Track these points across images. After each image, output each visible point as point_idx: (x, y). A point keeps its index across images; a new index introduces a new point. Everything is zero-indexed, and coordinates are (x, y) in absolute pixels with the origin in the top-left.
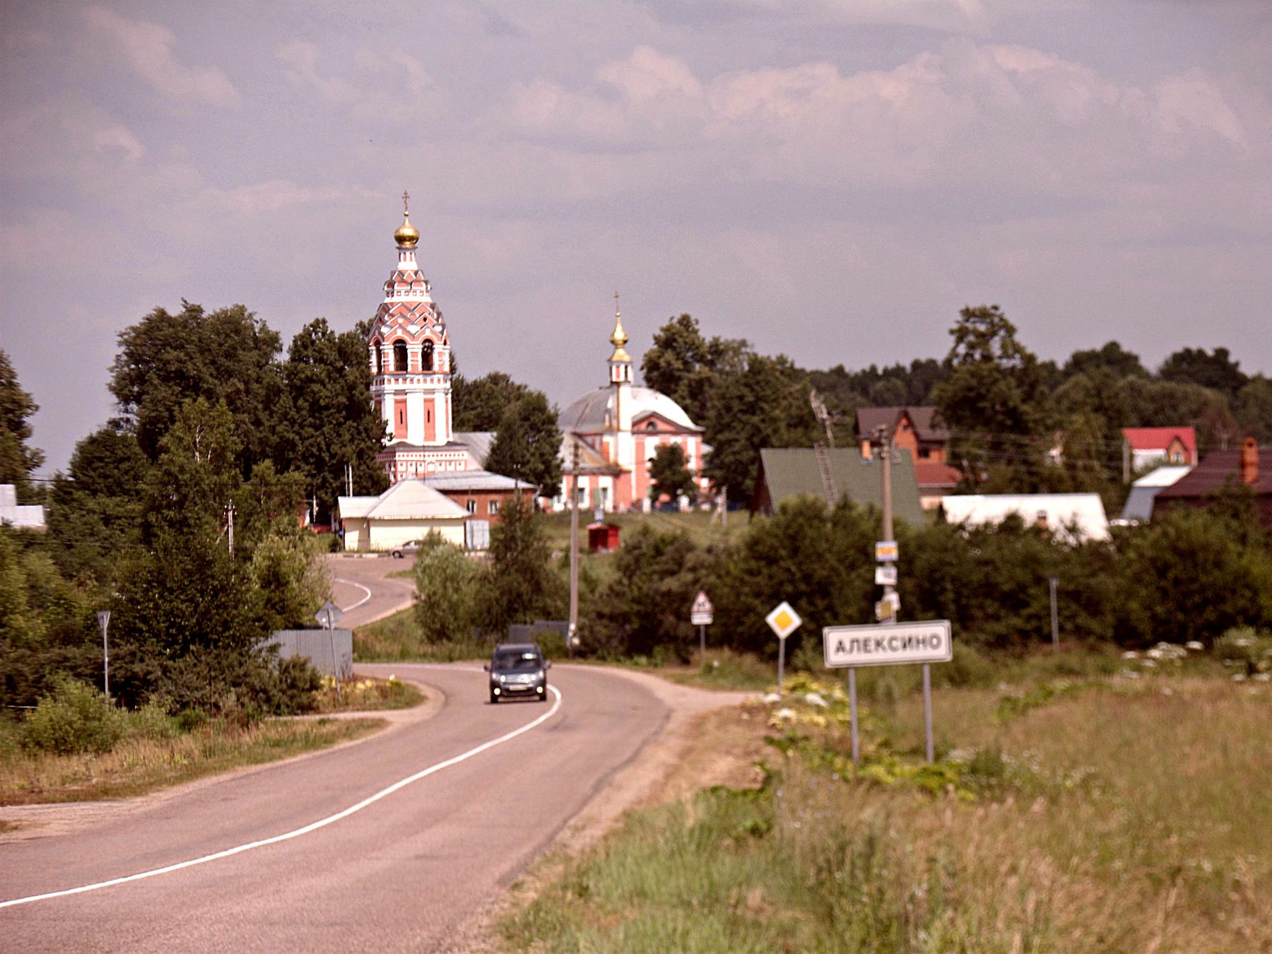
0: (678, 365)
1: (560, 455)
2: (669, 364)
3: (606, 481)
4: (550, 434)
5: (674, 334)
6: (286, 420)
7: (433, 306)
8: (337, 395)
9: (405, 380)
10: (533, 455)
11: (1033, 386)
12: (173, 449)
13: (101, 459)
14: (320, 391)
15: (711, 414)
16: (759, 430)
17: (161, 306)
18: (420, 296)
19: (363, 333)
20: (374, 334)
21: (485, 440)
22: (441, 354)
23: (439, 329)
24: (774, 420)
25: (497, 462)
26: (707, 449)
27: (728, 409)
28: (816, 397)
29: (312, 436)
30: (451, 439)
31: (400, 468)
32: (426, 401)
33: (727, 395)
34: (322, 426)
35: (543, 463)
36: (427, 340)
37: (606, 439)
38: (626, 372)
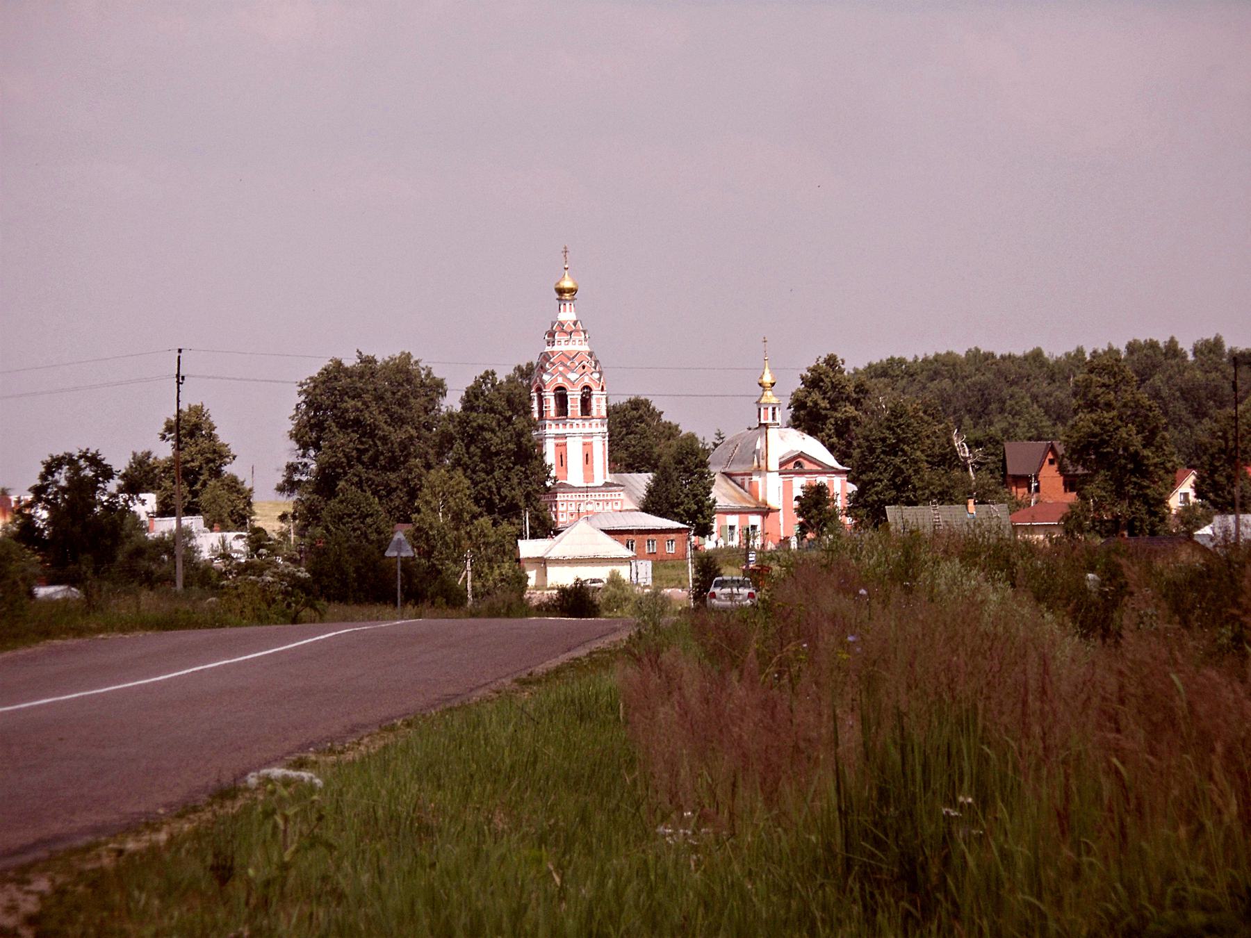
0: (824, 404)
1: (712, 496)
2: (816, 404)
3: (755, 520)
4: (702, 476)
5: (820, 374)
6: (460, 465)
7: (591, 354)
8: (507, 443)
9: (565, 425)
10: (687, 496)
11: (1153, 433)
12: (423, 510)
13: (349, 516)
14: (491, 439)
15: (856, 453)
16: (902, 472)
17: (338, 357)
18: (578, 345)
19: (521, 376)
20: (536, 382)
21: (642, 481)
22: (598, 400)
23: (596, 376)
24: (915, 462)
25: (653, 503)
26: (852, 488)
27: (872, 450)
28: (958, 435)
29: (484, 480)
30: (609, 480)
31: (561, 508)
32: (584, 444)
33: (871, 438)
34: (492, 471)
35: (696, 503)
36: (587, 387)
37: (755, 478)
38: (774, 414)
